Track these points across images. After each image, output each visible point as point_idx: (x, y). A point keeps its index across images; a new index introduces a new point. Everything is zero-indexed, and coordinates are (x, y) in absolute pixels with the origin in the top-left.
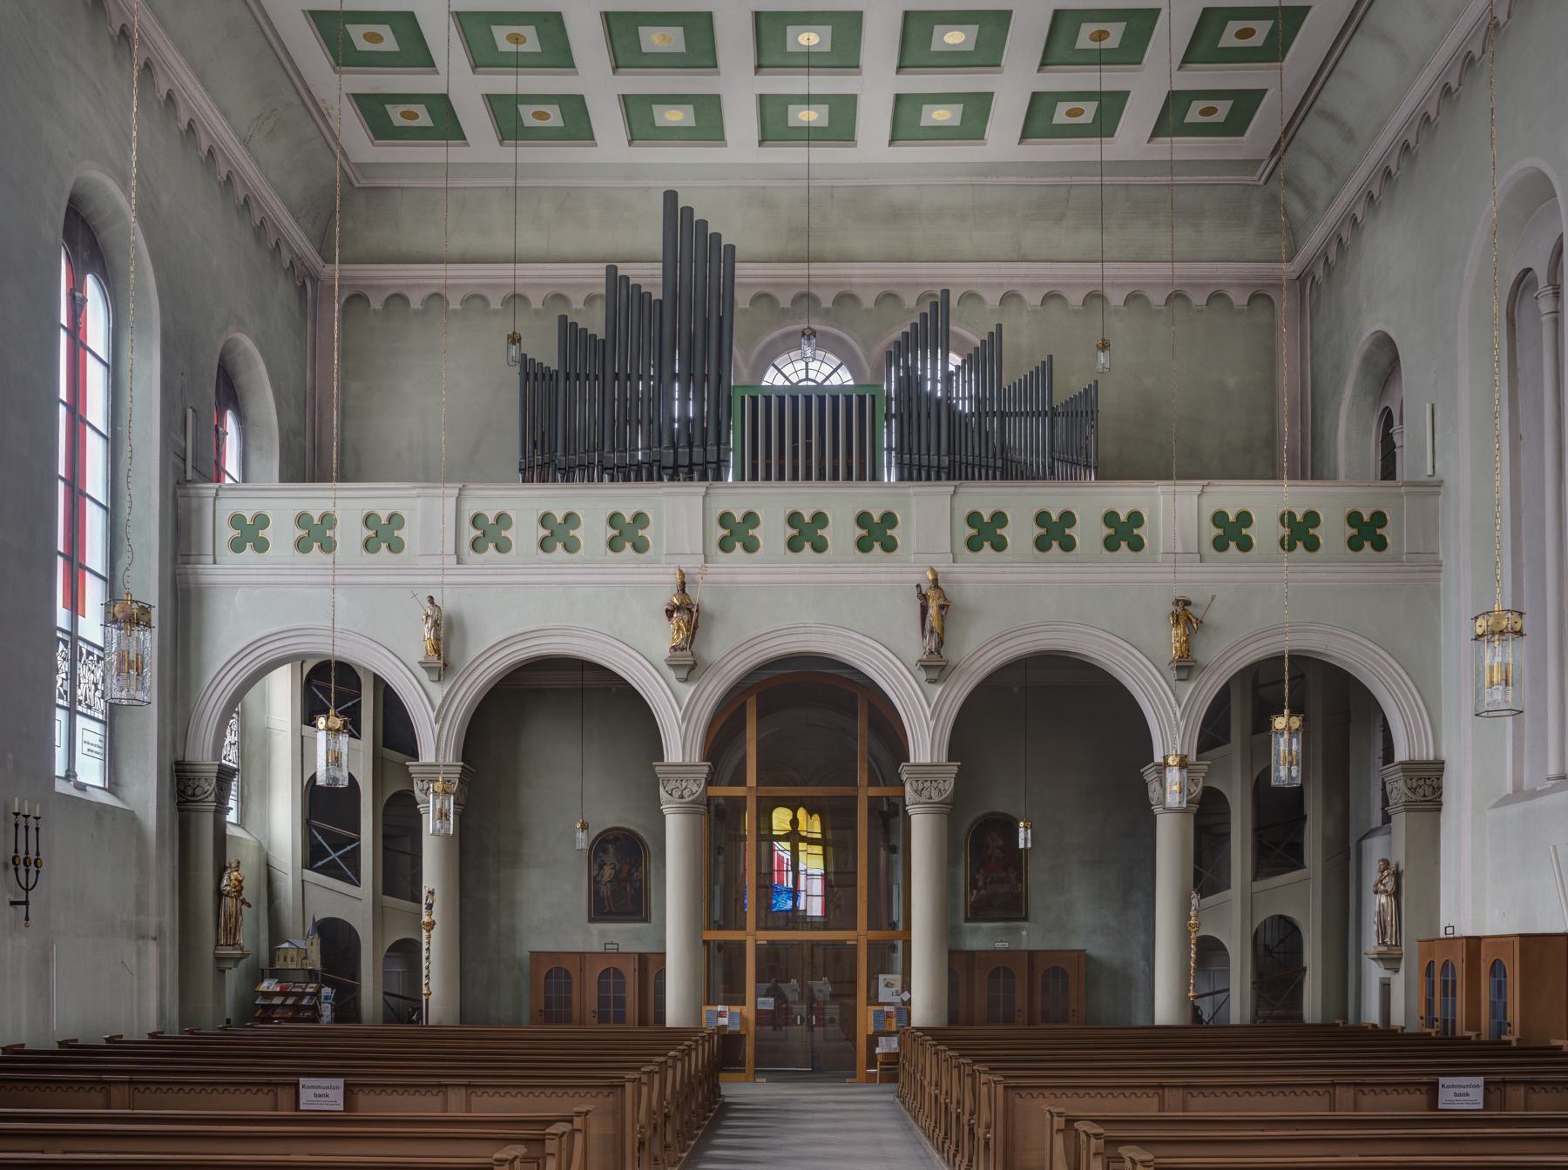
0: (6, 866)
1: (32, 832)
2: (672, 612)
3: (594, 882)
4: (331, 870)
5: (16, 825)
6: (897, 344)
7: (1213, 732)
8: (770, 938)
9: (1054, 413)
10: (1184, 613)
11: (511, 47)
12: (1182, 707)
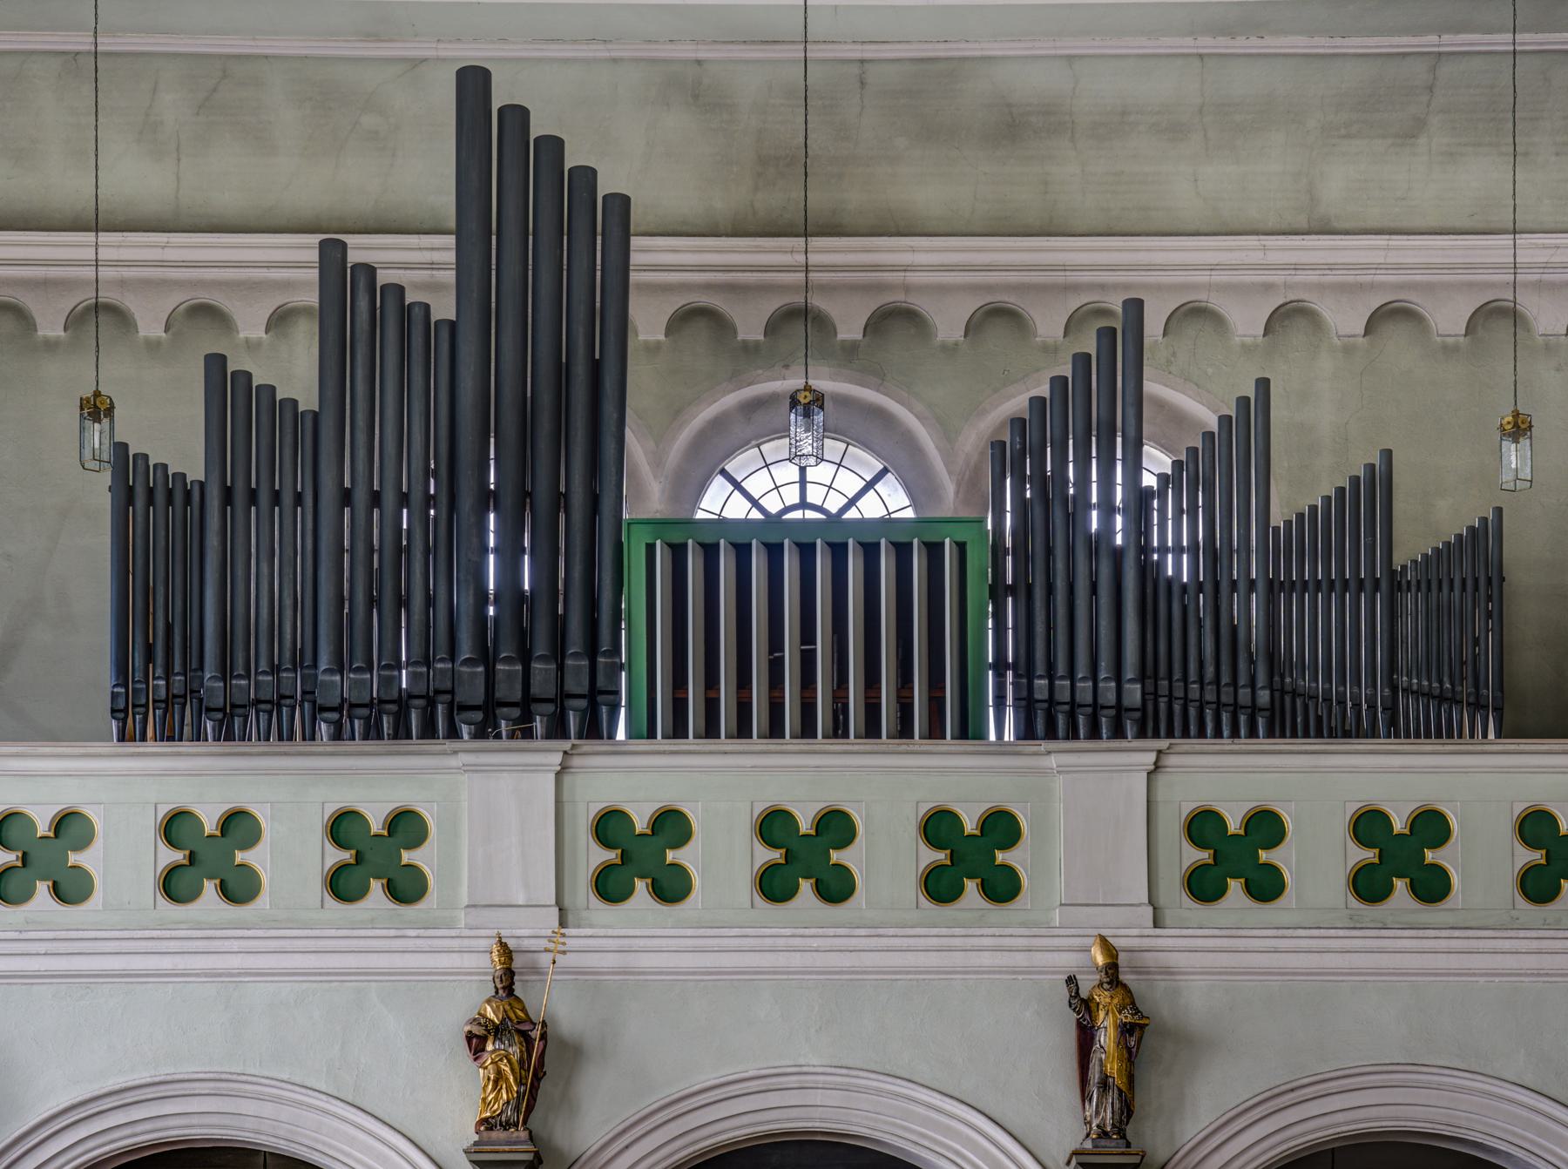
9: (1396, 583)
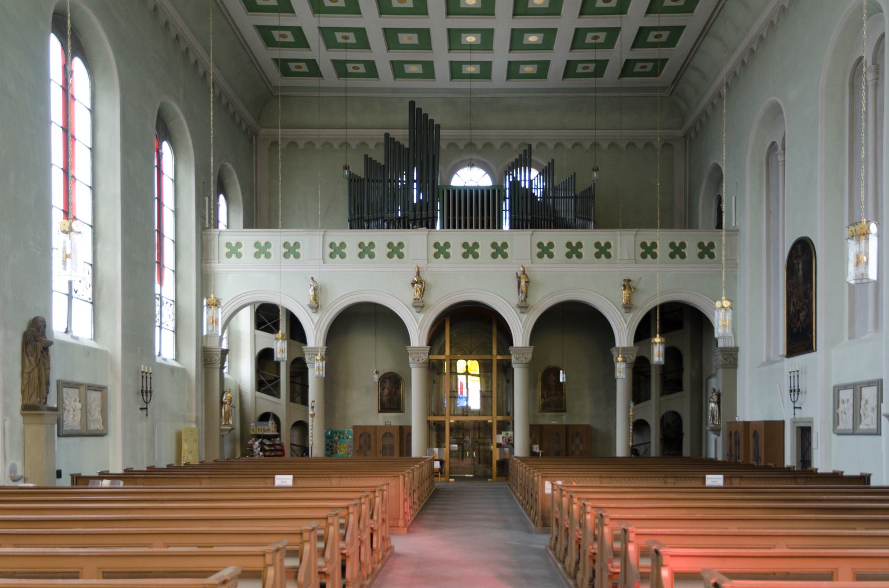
0: (138, 393)
1: (149, 379)
2: (414, 284)
3: (381, 395)
4: (268, 392)
5: (143, 377)
6: (513, 163)
7: (643, 333)
10: (628, 285)
11: (344, 41)
12: (627, 323)
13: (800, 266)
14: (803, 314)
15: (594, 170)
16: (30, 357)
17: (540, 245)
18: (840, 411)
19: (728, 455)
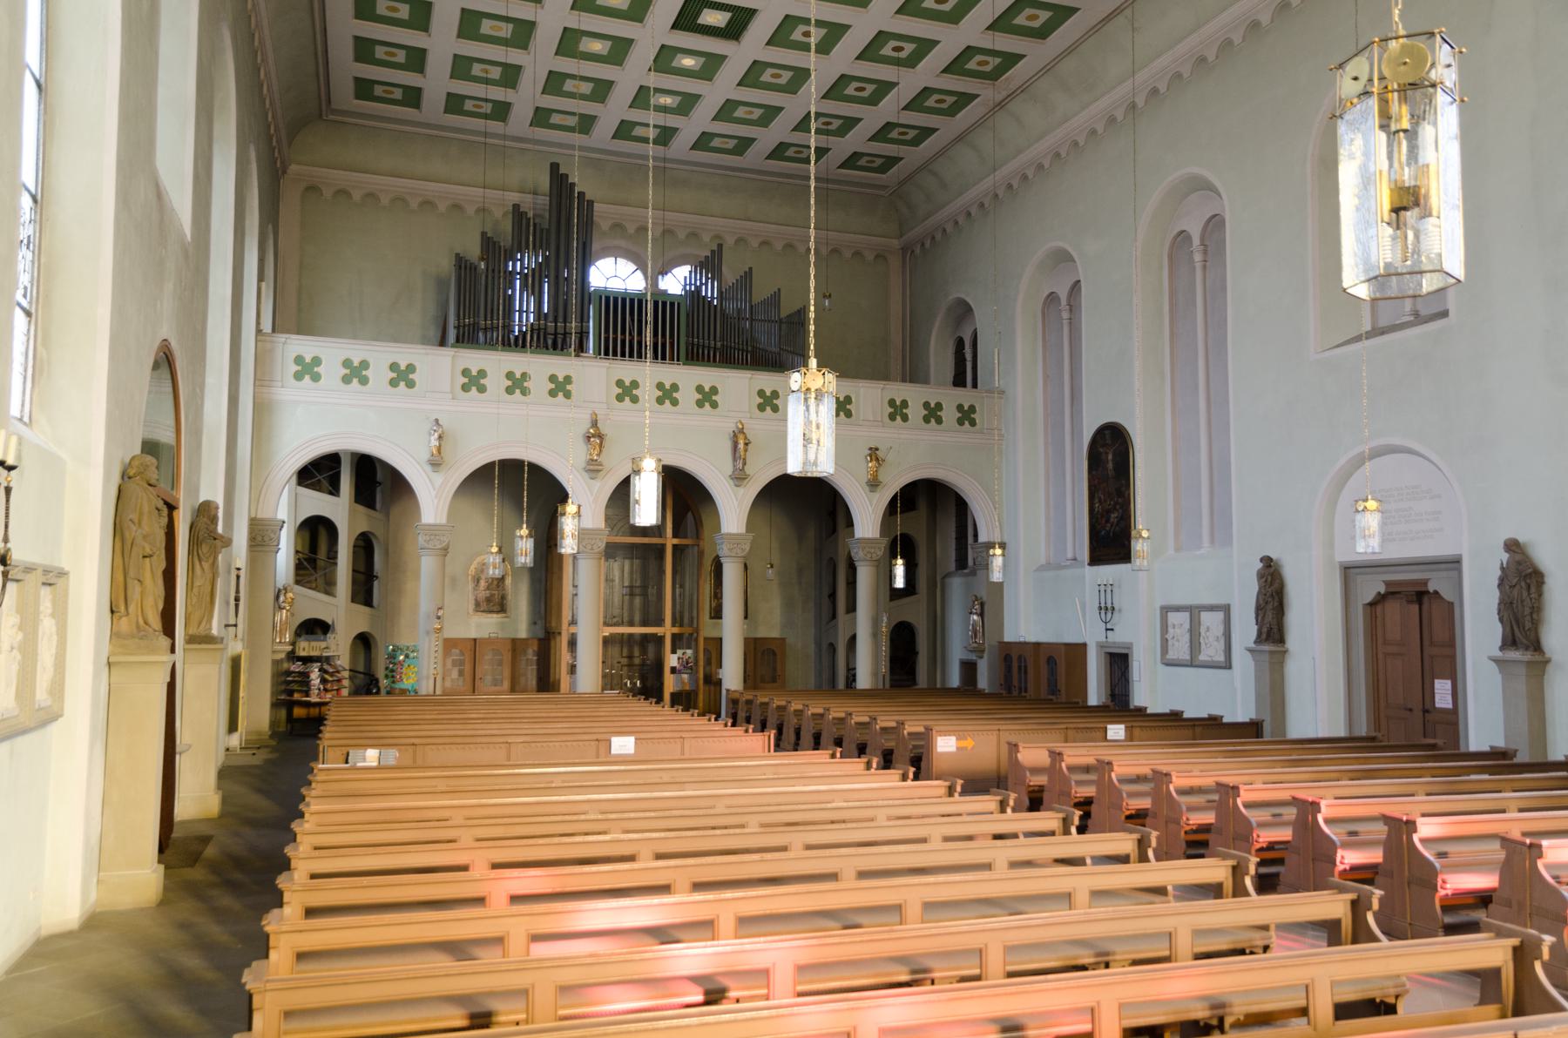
8: (612, 632)
9: (781, 321)
10: (874, 453)
13: (1110, 457)
14: (1116, 515)
15: (825, 296)
16: (203, 563)
17: (761, 393)
18: (1171, 636)
19: (1001, 685)
